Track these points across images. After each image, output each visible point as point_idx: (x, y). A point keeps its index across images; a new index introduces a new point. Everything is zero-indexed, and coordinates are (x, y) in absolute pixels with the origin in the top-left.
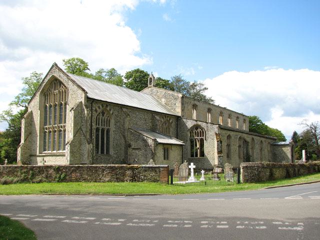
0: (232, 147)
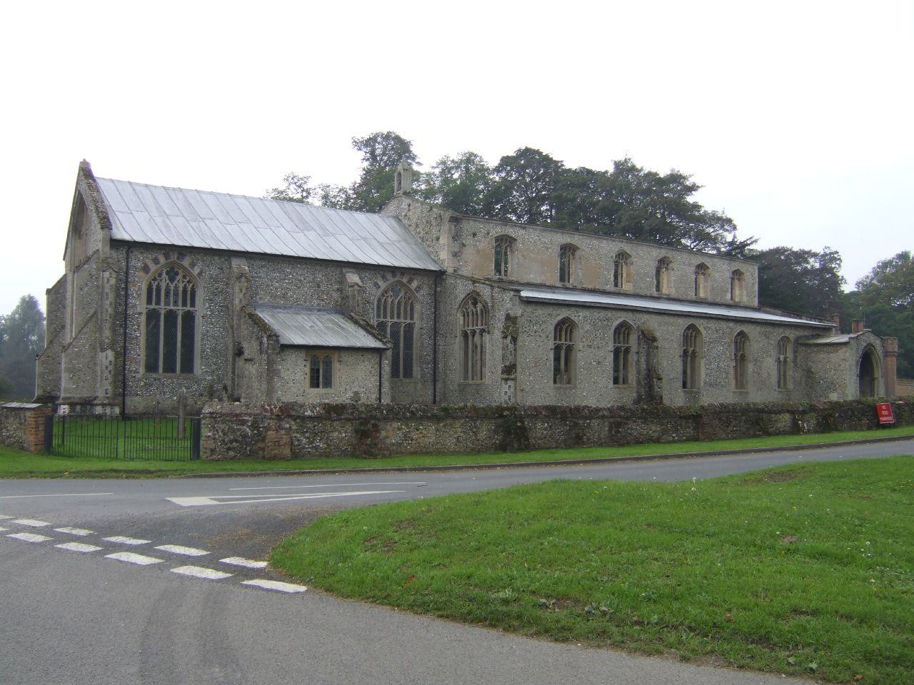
0: (579, 355)
